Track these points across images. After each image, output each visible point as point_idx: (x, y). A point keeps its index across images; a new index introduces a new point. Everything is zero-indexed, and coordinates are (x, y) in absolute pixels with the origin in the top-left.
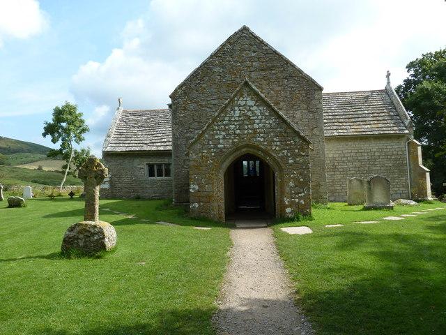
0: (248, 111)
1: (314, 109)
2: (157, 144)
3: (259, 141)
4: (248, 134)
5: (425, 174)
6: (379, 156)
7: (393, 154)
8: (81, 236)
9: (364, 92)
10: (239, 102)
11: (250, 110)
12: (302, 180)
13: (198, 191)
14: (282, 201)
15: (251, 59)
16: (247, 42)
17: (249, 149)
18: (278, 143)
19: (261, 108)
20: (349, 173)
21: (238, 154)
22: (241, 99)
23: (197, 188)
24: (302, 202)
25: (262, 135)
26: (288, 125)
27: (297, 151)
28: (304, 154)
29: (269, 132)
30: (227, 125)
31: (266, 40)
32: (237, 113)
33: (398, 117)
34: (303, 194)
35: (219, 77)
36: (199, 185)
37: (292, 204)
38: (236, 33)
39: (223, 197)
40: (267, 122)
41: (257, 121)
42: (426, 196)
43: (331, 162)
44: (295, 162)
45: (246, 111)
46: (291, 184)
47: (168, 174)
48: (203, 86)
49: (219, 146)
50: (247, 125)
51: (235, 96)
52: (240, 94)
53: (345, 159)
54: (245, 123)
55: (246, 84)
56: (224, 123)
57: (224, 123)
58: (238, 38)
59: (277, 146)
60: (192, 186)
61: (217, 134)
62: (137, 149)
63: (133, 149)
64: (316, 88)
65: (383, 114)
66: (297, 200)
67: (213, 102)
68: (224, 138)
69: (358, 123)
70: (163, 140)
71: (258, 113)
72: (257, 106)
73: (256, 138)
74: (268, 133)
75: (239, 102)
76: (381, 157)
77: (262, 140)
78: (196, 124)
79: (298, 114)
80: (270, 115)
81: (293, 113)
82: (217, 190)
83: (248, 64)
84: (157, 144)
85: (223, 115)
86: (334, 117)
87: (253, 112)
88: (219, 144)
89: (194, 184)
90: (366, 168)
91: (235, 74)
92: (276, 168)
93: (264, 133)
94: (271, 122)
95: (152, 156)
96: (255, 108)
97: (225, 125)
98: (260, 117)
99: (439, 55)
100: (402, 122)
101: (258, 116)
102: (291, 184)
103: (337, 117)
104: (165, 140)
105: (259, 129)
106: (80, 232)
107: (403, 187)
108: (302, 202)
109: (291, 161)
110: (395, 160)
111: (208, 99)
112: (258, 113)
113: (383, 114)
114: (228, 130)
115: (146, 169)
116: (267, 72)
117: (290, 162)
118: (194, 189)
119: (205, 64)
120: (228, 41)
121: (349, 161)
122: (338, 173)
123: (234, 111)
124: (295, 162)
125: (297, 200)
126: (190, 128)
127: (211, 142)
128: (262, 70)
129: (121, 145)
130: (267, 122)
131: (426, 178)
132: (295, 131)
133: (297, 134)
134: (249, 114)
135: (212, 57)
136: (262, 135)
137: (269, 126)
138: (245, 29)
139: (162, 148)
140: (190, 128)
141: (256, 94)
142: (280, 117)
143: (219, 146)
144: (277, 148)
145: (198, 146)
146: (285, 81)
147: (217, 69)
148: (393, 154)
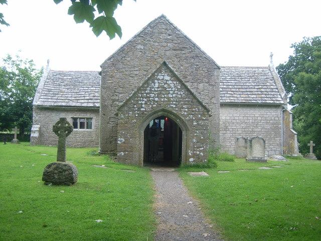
2: (81, 101)
3: (172, 107)
5: (294, 136)
7: (271, 120)
8: (56, 171)
9: (252, 68)
11: (166, 83)
12: (202, 138)
13: (124, 143)
14: (187, 153)
15: (167, 41)
16: (164, 27)
17: (164, 113)
18: (186, 110)
19: (175, 83)
22: (160, 74)
23: (123, 140)
24: (202, 154)
25: (174, 103)
26: (195, 97)
27: (200, 116)
28: (205, 119)
31: (179, 27)
32: (157, 85)
33: (277, 90)
34: (203, 148)
35: (140, 53)
36: (124, 138)
37: (194, 155)
39: (143, 149)
41: (171, 92)
43: (224, 123)
44: (198, 124)
45: (163, 84)
47: (89, 126)
49: (142, 109)
50: (164, 94)
51: (155, 72)
52: (159, 71)
53: (234, 121)
54: (167, 94)
55: (165, 63)
58: (157, 23)
59: (185, 111)
60: (119, 139)
62: (64, 104)
63: (60, 104)
64: (216, 67)
66: (198, 153)
67: (135, 73)
69: (246, 93)
70: (86, 98)
71: (172, 85)
72: (172, 81)
74: (179, 102)
78: (121, 89)
79: (201, 86)
80: (181, 88)
81: (197, 85)
82: (139, 143)
84: (81, 101)
86: (228, 87)
87: (168, 85)
88: (142, 107)
90: (250, 130)
91: (153, 51)
92: (183, 128)
93: (176, 101)
95: (76, 111)
96: (170, 82)
97: (147, 94)
99: (317, 42)
100: (280, 95)
101: (172, 88)
103: (231, 87)
104: (88, 98)
106: (55, 169)
107: (277, 145)
108: (202, 154)
109: (195, 123)
110: (273, 124)
112: (172, 85)
114: (149, 97)
118: (121, 141)
120: (149, 25)
122: (229, 132)
123: (155, 83)
124: (198, 124)
125: (198, 153)
126: (115, 92)
127: (135, 106)
129: (50, 100)
131: (294, 139)
132: (198, 101)
133: (201, 103)
134: (165, 86)
135: (135, 37)
136: (174, 103)
137: (180, 96)
138: (163, 16)
139: (85, 105)
140: (115, 92)
141: (171, 71)
142: (188, 90)
143: (142, 109)
146: (192, 60)
147: (139, 47)
148: (271, 120)
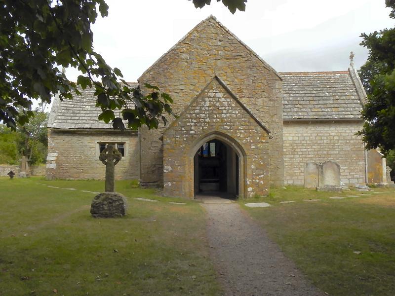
0: (217, 102)
1: (275, 98)
3: (226, 129)
4: (217, 122)
6: (338, 140)
7: (352, 139)
8: (105, 203)
10: (209, 94)
11: (219, 101)
12: (262, 163)
13: (172, 171)
14: (245, 181)
17: (217, 136)
20: (308, 156)
21: (208, 139)
22: (211, 91)
23: (170, 168)
27: (258, 138)
28: (264, 141)
29: (236, 122)
30: (198, 114)
32: (208, 103)
34: (262, 176)
36: (172, 166)
37: (253, 184)
38: (203, 22)
40: (234, 112)
42: (382, 181)
44: (257, 148)
46: (253, 167)
48: (171, 71)
49: (191, 132)
50: (216, 114)
56: (196, 112)
57: (196, 112)
59: (241, 133)
60: (165, 167)
61: (189, 122)
65: (344, 98)
66: (257, 181)
67: (181, 87)
68: (195, 125)
71: (226, 104)
72: (225, 98)
73: (223, 126)
75: (209, 94)
76: (340, 142)
77: (229, 128)
80: (236, 106)
83: (215, 52)
85: (194, 105)
87: (221, 103)
88: (191, 130)
89: (167, 165)
90: (325, 152)
93: (231, 122)
94: (237, 112)
96: (223, 100)
98: (227, 108)
101: (225, 107)
102: (253, 167)
105: (226, 118)
106: (104, 200)
111: (176, 84)
112: (226, 104)
113: (344, 98)
115: (98, 147)
116: (232, 61)
117: (252, 147)
118: (167, 170)
119: (173, 50)
120: (196, 29)
121: (309, 145)
122: (297, 156)
123: (205, 101)
124: (257, 148)
125: (257, 181)
127: (183, 129)
128: (227, 59)
129: (69, 121)
130: (234, 112)
131: (382, 163)
135: (179, 43)
136: (229, 123)
137: (235, 116)
143: (191, 132)
144: (242, 136)
145: (172, 132)
146: (249, 71)
147: (184, 56)
148: (352, 139)
